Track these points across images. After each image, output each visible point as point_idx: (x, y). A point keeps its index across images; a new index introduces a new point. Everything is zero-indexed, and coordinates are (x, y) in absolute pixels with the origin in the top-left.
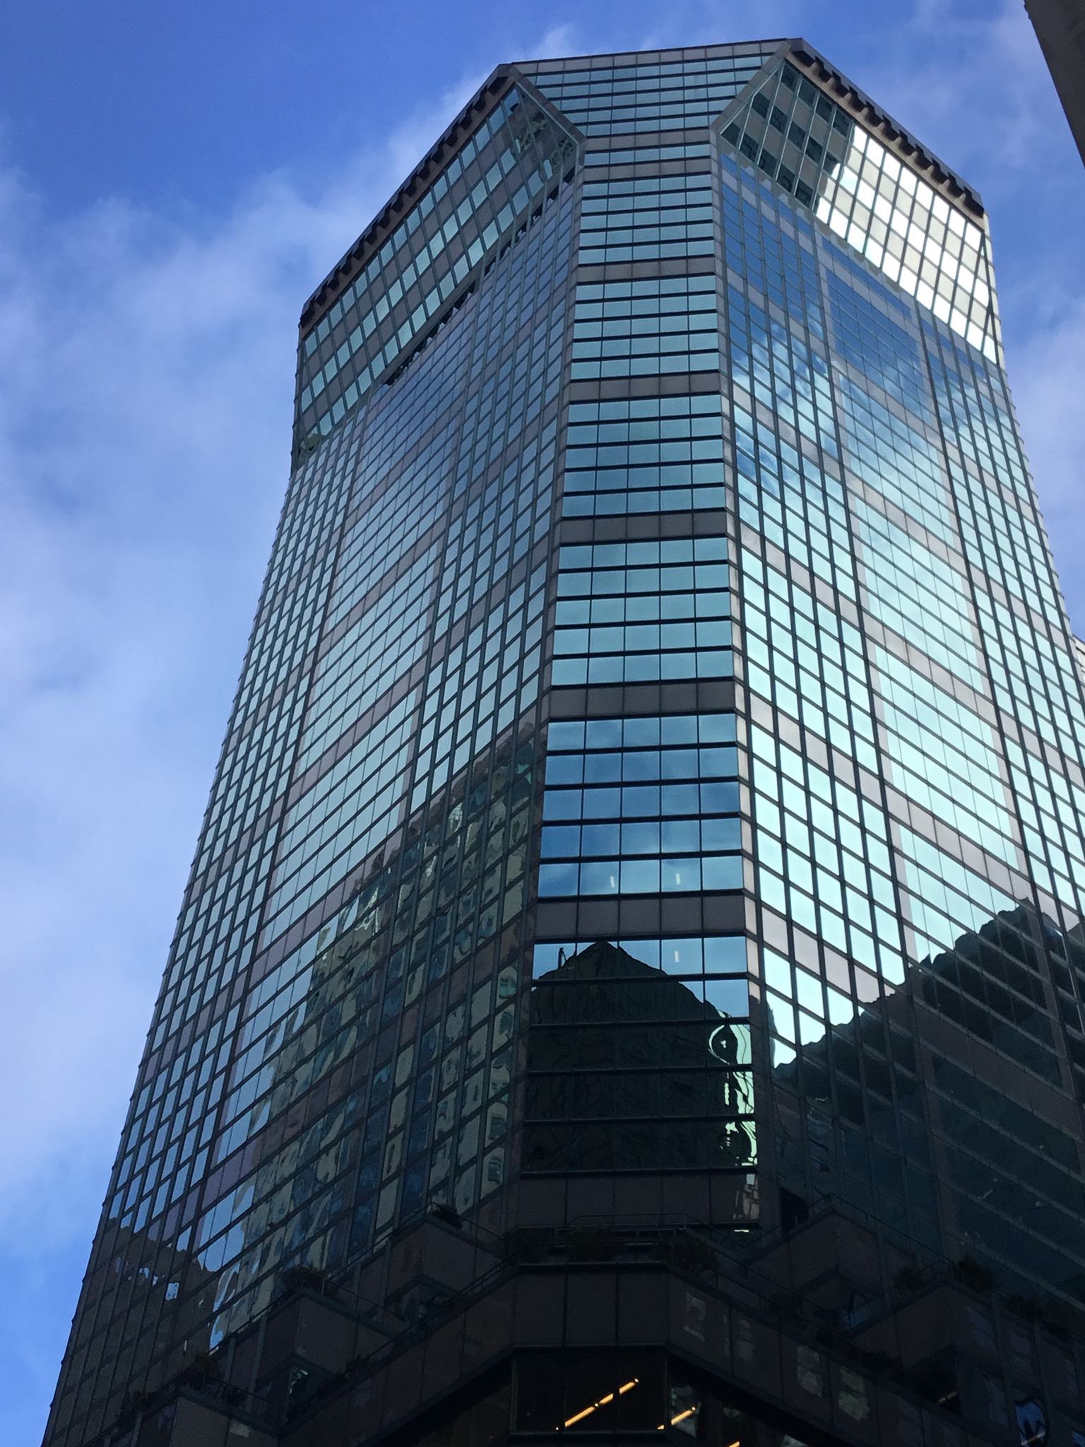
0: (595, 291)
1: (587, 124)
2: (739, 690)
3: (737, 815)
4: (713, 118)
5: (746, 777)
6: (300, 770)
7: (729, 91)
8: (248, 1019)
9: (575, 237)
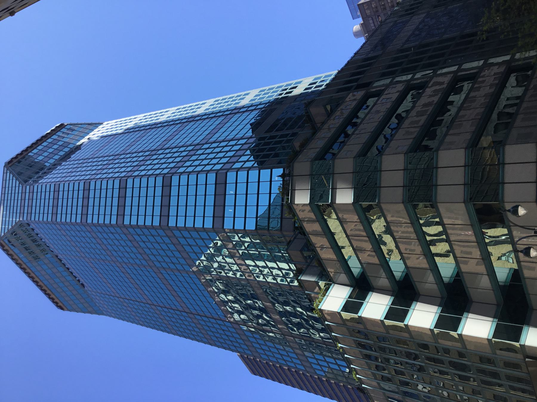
0: (90, 217)
7: (14, 181)
9: (36, 222)
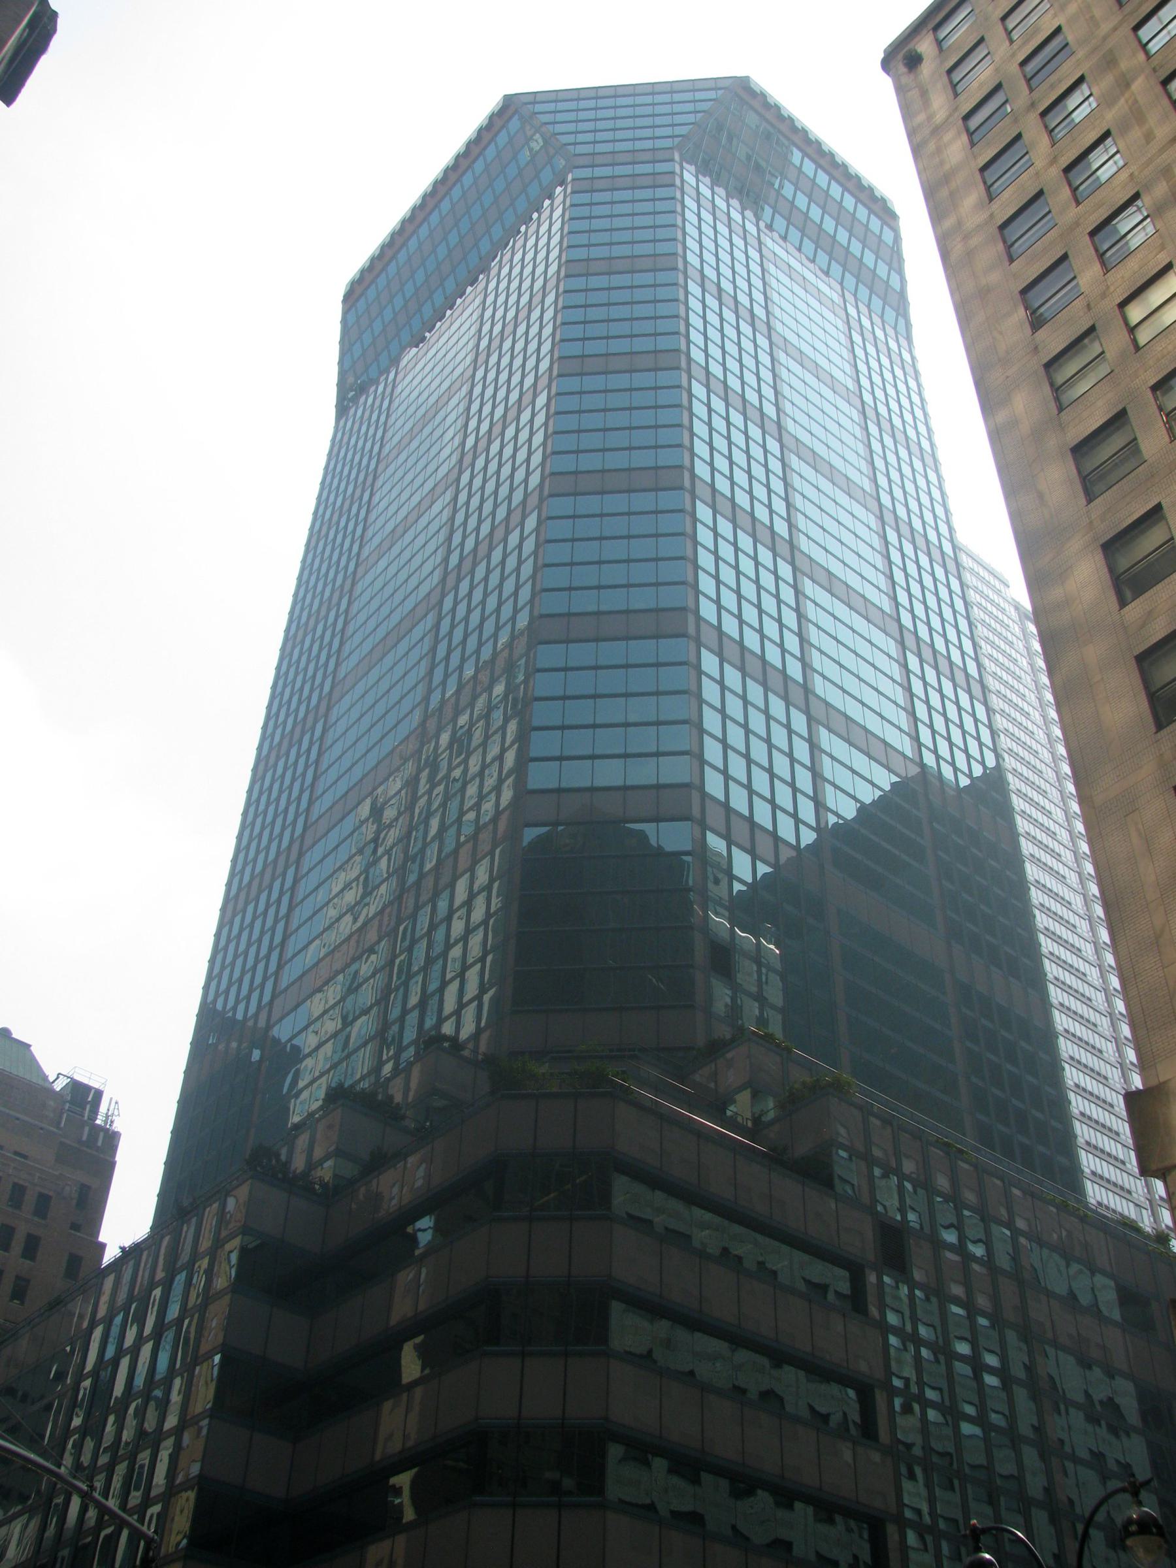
1: (575, 144)
2: (687, 475)
3: (679, 406)
4: (677, 140)
5: (691, 557)
6: (342, 673)
8: (317, 799)
